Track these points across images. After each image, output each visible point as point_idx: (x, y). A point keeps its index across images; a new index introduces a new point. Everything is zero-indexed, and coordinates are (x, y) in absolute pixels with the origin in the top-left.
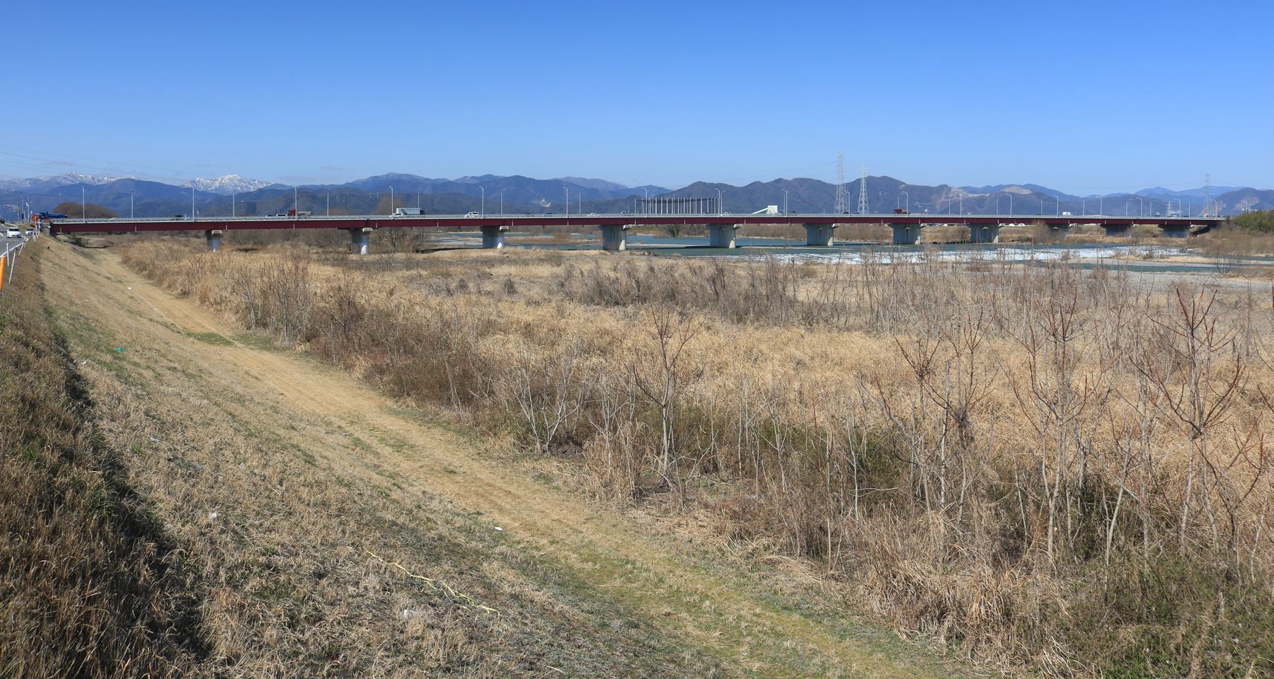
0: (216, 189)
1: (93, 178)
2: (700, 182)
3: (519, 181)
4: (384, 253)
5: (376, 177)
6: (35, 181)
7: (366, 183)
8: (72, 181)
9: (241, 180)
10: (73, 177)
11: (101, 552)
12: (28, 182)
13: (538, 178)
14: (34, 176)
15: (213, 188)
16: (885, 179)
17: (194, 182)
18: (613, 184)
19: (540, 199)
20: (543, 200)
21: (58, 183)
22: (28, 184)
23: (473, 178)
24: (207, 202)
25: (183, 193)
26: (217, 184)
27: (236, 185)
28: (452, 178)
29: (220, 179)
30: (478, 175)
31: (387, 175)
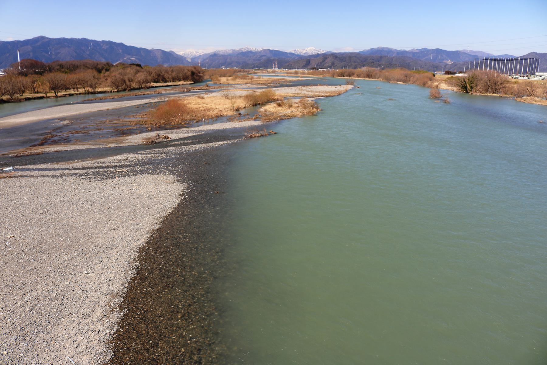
0: (304, 53)
1: (255, 49)
2: (534, 52)
3: (438, 51)
4: (143, 127)
5: (373, 49)
6: (233, 50)
7: (368, 51)
8: (247, 50)
9: (315, 50)
10: (248, 48)
11: (198, 279)
12: (231, 51)
13: (448, 49)
14: (233, 48)
15: (303, 53)
16: (109, 41)
17: (295, 50)
18: (487, 53)
19: (448, 60)
20: (450, 61)
21: (242, 51)
22: (231, 52)
23: (417, 49)
24: (296, 59)
25: (289, 55)
26: (305, 51)
27: (312, 52)
28: (407, 50)
29: (306, 49)
30: (420, 48)
31: (378, 48)
